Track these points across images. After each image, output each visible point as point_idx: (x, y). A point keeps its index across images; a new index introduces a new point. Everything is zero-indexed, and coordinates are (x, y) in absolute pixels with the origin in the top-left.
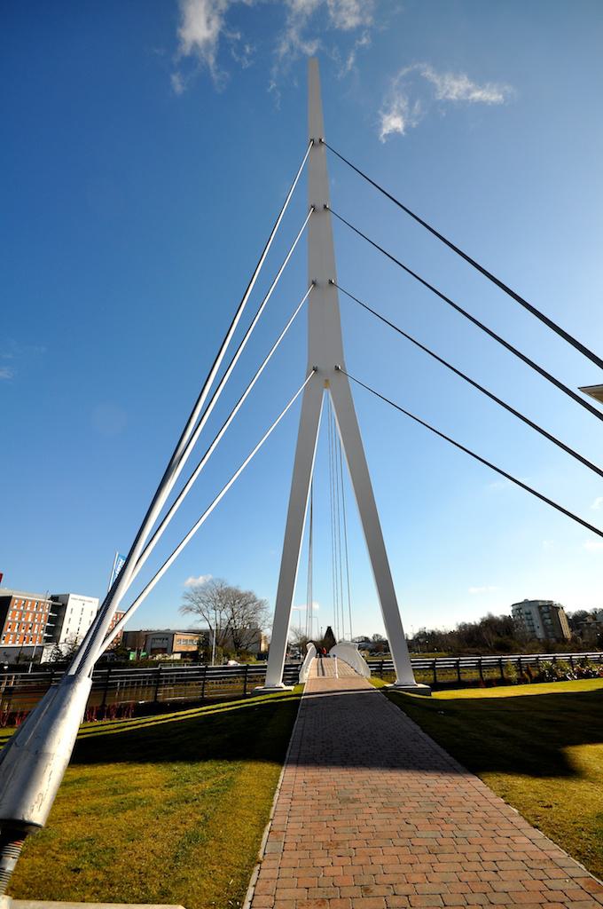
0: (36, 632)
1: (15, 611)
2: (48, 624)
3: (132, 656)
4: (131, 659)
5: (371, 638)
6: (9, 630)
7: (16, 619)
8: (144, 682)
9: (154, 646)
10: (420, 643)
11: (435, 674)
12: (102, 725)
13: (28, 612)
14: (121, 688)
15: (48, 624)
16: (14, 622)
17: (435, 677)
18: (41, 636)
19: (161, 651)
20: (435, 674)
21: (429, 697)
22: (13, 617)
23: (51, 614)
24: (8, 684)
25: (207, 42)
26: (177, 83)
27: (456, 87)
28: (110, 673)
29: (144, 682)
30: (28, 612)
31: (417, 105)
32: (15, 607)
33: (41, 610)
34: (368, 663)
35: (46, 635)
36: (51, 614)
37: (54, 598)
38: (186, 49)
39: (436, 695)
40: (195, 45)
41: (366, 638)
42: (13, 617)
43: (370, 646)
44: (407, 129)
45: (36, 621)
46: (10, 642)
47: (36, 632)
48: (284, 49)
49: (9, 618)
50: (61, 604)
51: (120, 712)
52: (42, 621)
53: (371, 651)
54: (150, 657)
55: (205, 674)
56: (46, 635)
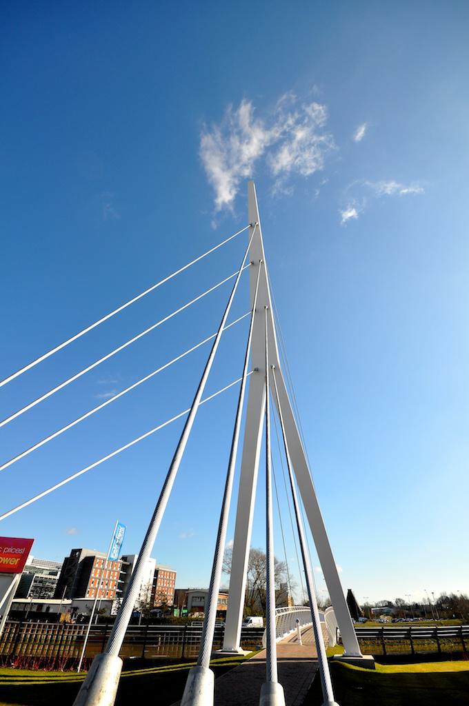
0: (110, 587)
1: (97, 569)
2: (120, 581)
3: (176, 613)
4: (175, 615)
5: (394, 602)
6: (92, 585)
7: (97, 576)
8: (180, 639)
9: (194, 604)
10: (442, 610)
11: (412, 644)
12: (56, 676)
13: (106, 570)
14: (162, 643)
15: (120, 581)
16: (96, 579)
17: (412, 647)
18: (114, 591)
19: (197, 609)
20: (412, 644)
21: (373, 671)
22: (95, 575)
23: (121, 572)
24: (78, 634)
25: (229, 201)
26: (214, 225)
27: (390, 187)
28: (148, 628)
29: (176, 639)
30: (106, 570)
31: (365, 201)
32: (97, 565)
33: (114, 568)
34: (356, 630)
35: (118, 590)
36: (121, 572)
37: (124, 558)
38: (219, 208)
39: (380, 668)
40: (224, 203)
41: (390, 603)
42: (95, 574)
43: (393, 611)
44: (359, 214)
45: (111, 577)
46: (93, 596)
47: (110, 587)
48: (274, 192)
49: (92, 575)
50: (128, 564)
51: (26, 662)
52: (115, 578)
53: (394, 616)
54: (190, 614)
55: (147, 633)
56: (118, 590)
